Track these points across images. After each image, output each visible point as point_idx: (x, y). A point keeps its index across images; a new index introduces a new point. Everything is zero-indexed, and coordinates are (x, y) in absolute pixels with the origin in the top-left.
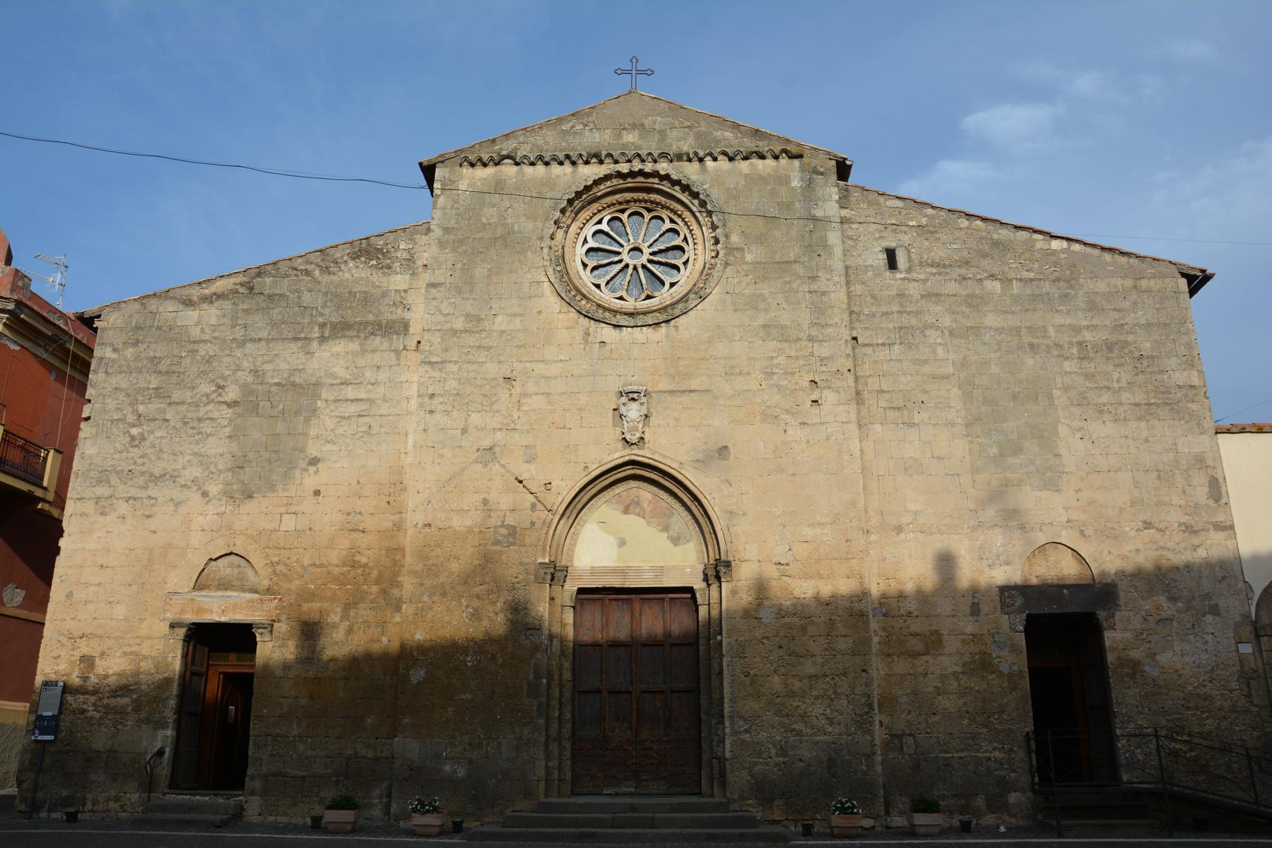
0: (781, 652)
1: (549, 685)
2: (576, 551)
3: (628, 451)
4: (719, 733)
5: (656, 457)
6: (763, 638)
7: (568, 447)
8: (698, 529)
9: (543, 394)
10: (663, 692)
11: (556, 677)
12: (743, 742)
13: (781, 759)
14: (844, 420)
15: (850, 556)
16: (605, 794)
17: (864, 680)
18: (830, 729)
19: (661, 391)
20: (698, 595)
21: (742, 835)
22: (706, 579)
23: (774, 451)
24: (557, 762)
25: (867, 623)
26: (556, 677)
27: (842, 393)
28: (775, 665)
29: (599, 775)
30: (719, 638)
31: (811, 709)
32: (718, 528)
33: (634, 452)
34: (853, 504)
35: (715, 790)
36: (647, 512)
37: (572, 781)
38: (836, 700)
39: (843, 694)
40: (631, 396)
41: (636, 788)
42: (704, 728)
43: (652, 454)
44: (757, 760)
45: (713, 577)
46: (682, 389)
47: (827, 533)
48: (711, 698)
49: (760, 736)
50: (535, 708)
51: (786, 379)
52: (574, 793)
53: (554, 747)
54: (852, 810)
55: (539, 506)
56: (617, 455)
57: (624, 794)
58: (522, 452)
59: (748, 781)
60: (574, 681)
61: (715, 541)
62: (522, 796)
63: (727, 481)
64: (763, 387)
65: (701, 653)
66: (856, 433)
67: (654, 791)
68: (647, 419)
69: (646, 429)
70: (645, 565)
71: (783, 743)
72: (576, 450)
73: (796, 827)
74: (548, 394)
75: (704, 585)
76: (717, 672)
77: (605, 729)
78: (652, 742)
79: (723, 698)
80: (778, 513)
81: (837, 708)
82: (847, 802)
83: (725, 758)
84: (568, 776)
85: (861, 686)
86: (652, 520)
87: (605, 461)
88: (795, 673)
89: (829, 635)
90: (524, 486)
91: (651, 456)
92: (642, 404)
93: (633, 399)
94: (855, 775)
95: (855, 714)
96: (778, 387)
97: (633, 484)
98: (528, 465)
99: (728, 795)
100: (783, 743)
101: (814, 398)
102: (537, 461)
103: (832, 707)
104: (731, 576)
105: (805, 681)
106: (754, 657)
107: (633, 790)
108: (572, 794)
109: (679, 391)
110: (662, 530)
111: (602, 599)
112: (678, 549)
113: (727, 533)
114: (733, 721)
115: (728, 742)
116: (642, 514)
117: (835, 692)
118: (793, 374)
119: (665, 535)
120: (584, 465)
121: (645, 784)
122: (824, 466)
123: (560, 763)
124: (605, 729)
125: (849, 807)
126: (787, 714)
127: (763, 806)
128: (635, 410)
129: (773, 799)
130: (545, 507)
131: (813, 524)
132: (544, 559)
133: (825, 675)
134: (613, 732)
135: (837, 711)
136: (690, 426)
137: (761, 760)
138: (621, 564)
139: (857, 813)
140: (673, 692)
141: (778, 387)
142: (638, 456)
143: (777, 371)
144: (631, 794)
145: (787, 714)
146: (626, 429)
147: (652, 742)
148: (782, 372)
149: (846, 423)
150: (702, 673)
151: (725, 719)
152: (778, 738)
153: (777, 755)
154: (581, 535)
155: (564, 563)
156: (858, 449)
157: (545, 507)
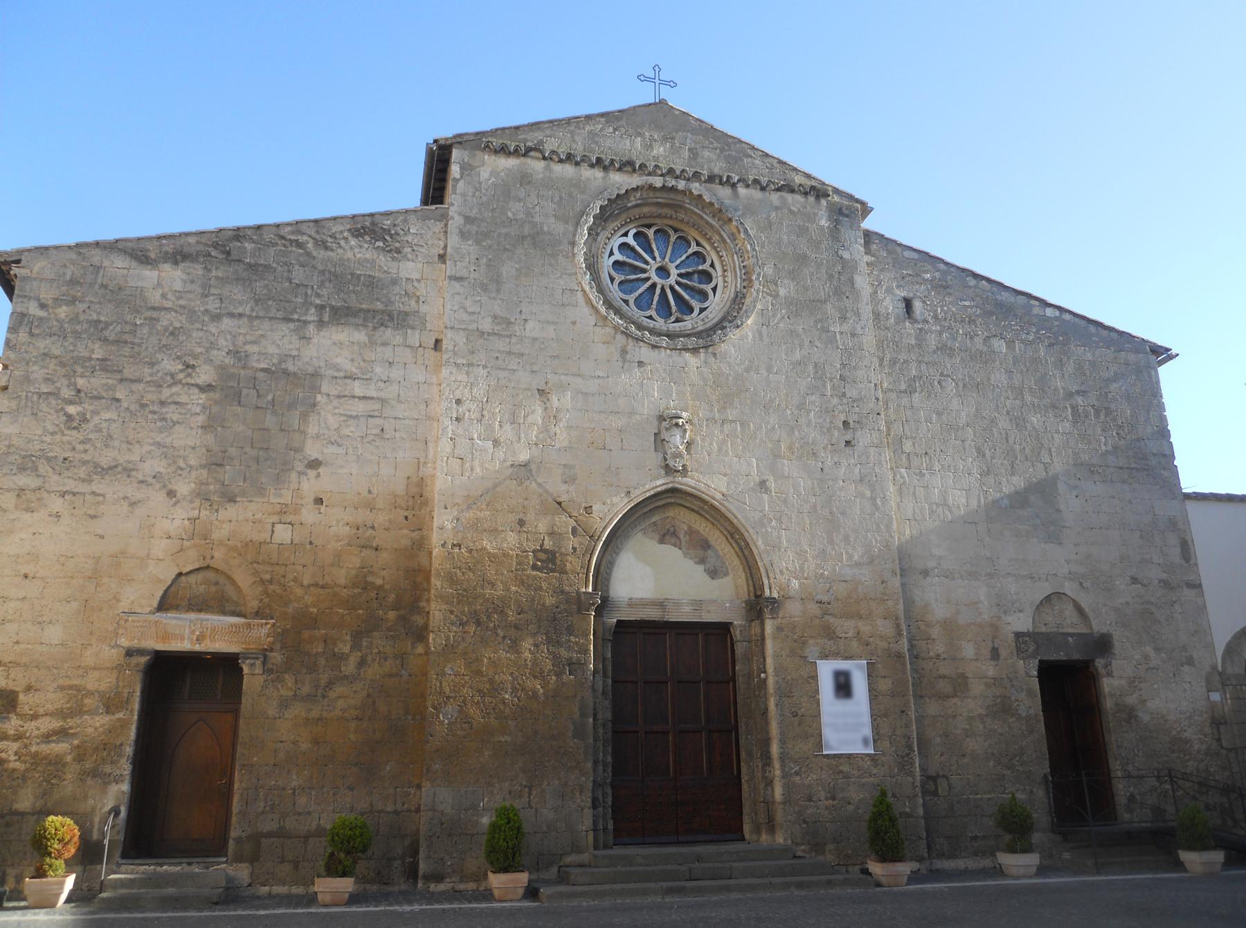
2: (612, 581)
15: (886, 598)
49: (810, 778)
72: (618, 474)
101: (848, 438)
112: (716, 582)
119: (701, 567)
129: (825, 844)
153: (827, 799)
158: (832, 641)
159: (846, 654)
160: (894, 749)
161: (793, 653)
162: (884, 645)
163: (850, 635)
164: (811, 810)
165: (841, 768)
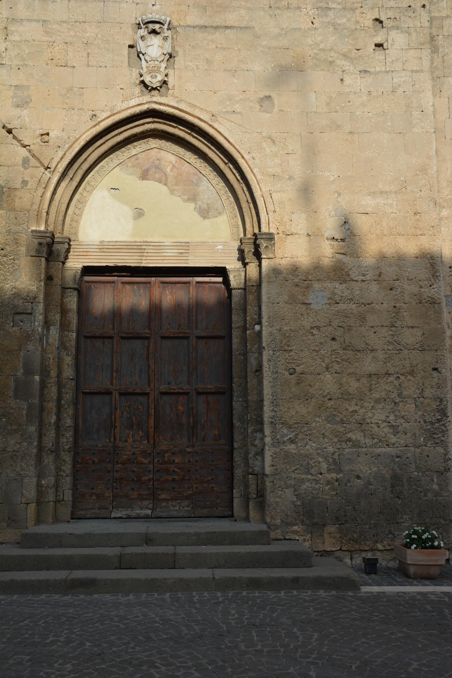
0: (335, 345)
1: (43, 385)
2: (82, 223)
3: (147, 98)
4: (256, 442)
5: (182, 106)
6: (312, 328)
7: (71, 89)
8: (232, 199)
9: (39, 21)
10: (187, 393)
11: (53, 373)
12: (287, 455)
13: (334, 475)
14: (415, 69)
15: (419, 232)
16: (115, 518)
17: (436, 380)
18: (393, 439)
19: (189, 26)
20: (231, 277)
21: (296, 580)
22: (242, 258)
23: (328, 104)
24: (52, 479)
25: (439, 313)
26: (53, 373)
27: (414, 34)
28: (327, 361)
29: (107, 494)
30: (257, 327)
31: (370, 415)
32: (257, 194)
33: (154, 99)
34: (424, 170)
35: (251, 513)
36: (169, 180)
37: (73, 501)
38: (401, 404)
39: (409, 397)
40: (151, 26)
41: (153, 509)
42: (237, 436)
43: (178, 102)
44: (303, 476)
45: (251, 254)
46: (215, 25)
47: (392, 204)
48: (247, 401)
49: (308, 447)
50: (25, 412)
51: (345, 16)
52: (75, 517)
53: (49, 460)
54: (433, 542)
55: (33, 162)
56: (133, 102)
57: (138, 518)
58: (11, 93)
59: (293, 502)
60: (77, 379)
61: (254, 212)
62: (4, 524)
63: (270, 138)
64: (316, 25)
65: (234, 346)
66: (429, 84)
67: (175, 514)
68: (171, 60)
69: (171, 72)
70: (168, 241)
71: (336, 456)
72: (81, 95)
73: (351, 559)
74: (44, 21)
75: (239, 265)
76: (254, 369)
77: (115, 439)
78: (173, 453)
79: (262, 400)
80: (332, 178)
81: (403, 413)
82: (424, 532)
83: (264, 474)
84: (68, 496)
85: (432, 387)
86: (177, 188)
87: (119, 109)
88: (352, 370)
89: (393, 326)
90: (15, 137)
91: (176, 105)
92: (165, 39)
93: (154, 32)
94: (425, 495)
95: (425, 422)
96: (335, 26)
97: (153, 143)
98: (18, 110)
99: (268, 520)
100: (336, 456)
101: (378, 40)
102: (30, 105)
103: (397, 413)
104: (274, 253)
105: (364, 380)
106: (302, 350)
107: (149, 512)
108: (72, 518)
109: (212, 27)
110: (189, 200)
111: (113, 282)
112: (207, 222)
113: (268, 200)
114: (275, 428)
115: (268, 455)
116: (164, 179)
117: (399, 395)
118: (353, 10)
119: (192, 205)
120: (91, 113)
121: (164, 504)
122: (389, 124)
123: (57, 481)
124: (115, 439)
125: (427, 538)
126: (342, 420)
127: (311, 533)
128: (156, 46)
129: (324, 525)
130: (41, 163)
131: (374, 193)
132: (39, 225)
133: (388, 374)
134: (126, 441)
135: (403, 417)
136: (225, 70)
137: (309, 477)
138: (138, 239)
139: (439, 547)
140: (199, 393)
141: (335, 26)
142: (160, 104)
143: (334, 6)
144: (146, 517)
145: (342, 420)
146: (145, 70)
147: (173, 453)
148: (339, 7)
149: (417, 71)
150: (236, 369)
151: (265, 426)
152: (331, 449)
153: (329, 470)
154: (88, 204)
155: (66, 234)
156: (431, 104)
157: (41, 163)
158: (344, 285)
159: (362, 301)
160: (420, 413)
161: (292, 300)
162: (415, 289)
163: (368, 277)
164: (307, 484)
165: (350, 435)
